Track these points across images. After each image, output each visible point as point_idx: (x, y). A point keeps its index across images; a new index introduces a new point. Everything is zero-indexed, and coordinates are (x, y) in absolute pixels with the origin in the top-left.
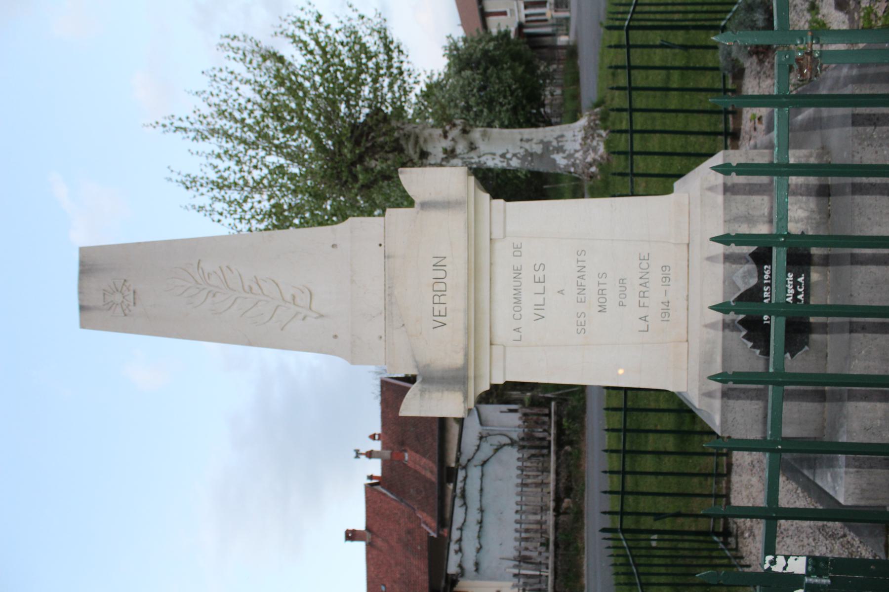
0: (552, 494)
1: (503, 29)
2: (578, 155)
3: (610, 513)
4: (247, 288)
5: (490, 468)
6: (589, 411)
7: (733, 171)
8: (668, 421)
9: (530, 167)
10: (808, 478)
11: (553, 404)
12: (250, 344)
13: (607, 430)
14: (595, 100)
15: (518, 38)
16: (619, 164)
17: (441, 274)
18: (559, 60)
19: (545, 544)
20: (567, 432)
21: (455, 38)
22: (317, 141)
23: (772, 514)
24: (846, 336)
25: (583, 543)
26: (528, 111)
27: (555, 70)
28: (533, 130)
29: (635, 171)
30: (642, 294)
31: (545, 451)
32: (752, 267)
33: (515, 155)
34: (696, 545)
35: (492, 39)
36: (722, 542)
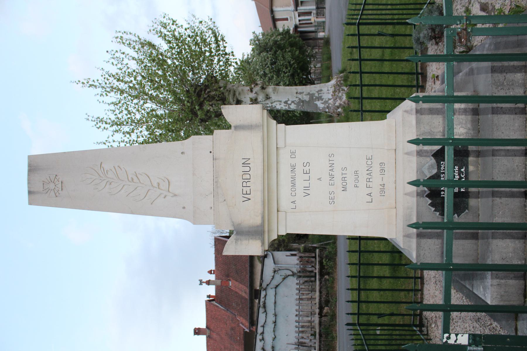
0: (317, 304)
1: (286, 29)
2: (330, 102)
3: (351, 314)
4: (130, 179)
5: (280, 289)
6: (338, 254)
7: (421, 100)
8: (386, 258)
9: (303, 110)
10: (469, 289)
11: (317, 250)
12: (132, 213)
13: (349, 264)
14: (341, 69)
15: (295, 34)
16: (355, 105)
17: (247, 169)
18: (319, 46)
19: (314, 335)
20: (326, 267)
21: (258, 34)
22: (174, 93)
23: (447, 309)
24: (490, 199)
25: (336, 333)
26: (300, 75)
27: (316, 53)
28: (304, 87)
29: (364, 109)
30: (368, 180)
31: (313, 279)
32: (433, 161)
33: (293, 102)
34: (404, 333)
35: (280, 34)
36: (419, 331)
